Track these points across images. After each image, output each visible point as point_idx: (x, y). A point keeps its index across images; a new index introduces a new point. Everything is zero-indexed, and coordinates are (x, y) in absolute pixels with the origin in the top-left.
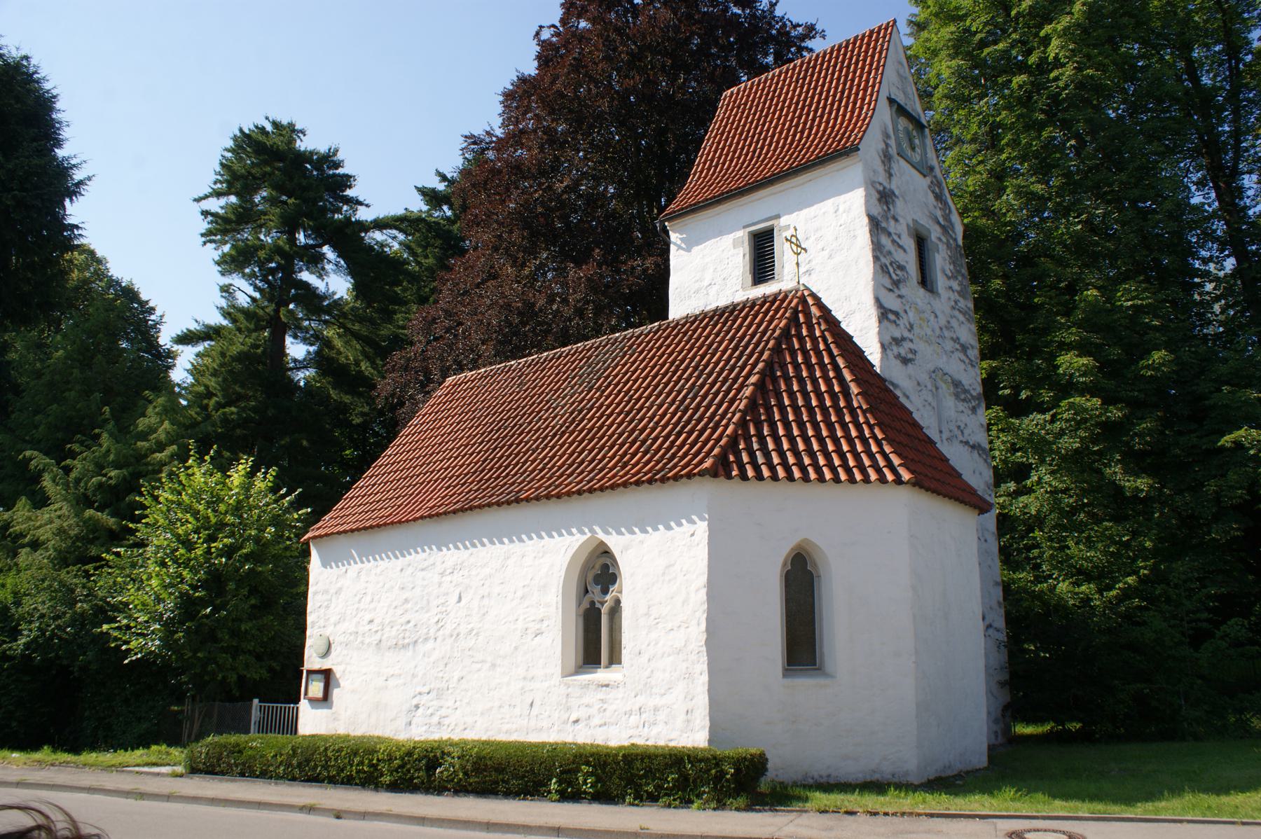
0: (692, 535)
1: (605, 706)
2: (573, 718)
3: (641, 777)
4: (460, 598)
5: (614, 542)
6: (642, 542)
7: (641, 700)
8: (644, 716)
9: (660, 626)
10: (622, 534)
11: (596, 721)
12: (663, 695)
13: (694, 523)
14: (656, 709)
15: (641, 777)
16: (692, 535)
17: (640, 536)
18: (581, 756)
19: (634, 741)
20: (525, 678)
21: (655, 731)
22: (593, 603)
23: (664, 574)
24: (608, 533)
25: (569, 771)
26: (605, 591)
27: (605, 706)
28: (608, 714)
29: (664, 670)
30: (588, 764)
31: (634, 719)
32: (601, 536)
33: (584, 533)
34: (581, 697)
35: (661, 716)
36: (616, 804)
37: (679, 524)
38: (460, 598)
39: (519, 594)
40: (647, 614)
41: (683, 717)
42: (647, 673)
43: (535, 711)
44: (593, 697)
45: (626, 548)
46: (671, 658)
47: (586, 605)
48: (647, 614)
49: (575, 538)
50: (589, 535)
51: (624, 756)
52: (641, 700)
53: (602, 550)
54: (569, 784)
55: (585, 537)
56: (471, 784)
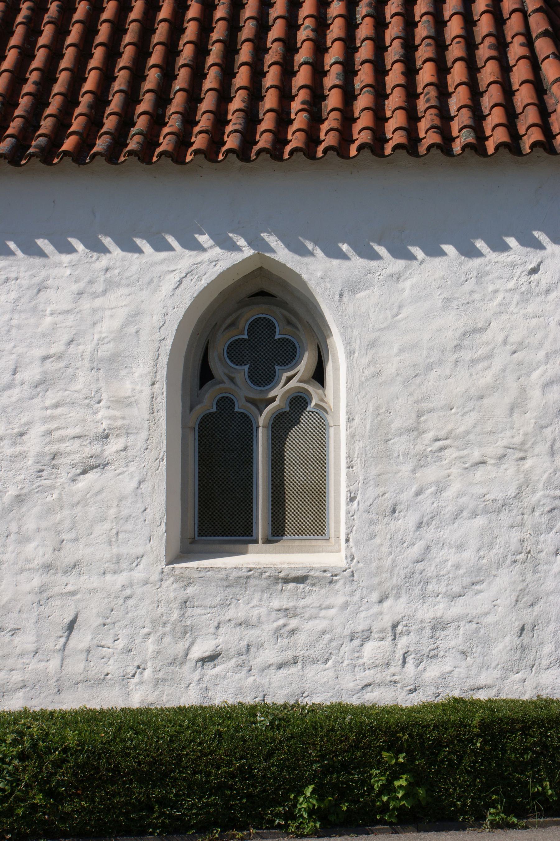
0: (534, 271)
1: (293, 623)
2: (201, 649)
3: (522, 767)
4: (415, 376)
5: (319, 273)
6: (397, 277)
7: (395, 608)
8: (403, 642)
9: (450, 454)
10: (344, 257)
11: (269, 655)
12: (454, 597)
13: (540, 246)
14: (438, 626)
15: (522, 767)
16: (534, 271)
17: (391, 264)
18: (373, 731)
19: (240, 699)
20: (48, 567)
21: (433, 672)
22: (226, 403)
23: (458, 347)
24: (302, 251)
25: (345, 767)
26: (264, 377)
27: (293, 623)
28: (301, 638)
29: (461, 547)
30: (394, 746)
31: (371, 649)
32: (282, 254)
33: (235, 248)
34: (224, 605)
35: (451, 640)
36: (462, 827)
37: (500, 247)
38: (415, 376)
39: (31, 373)
40: (416, 430)
41: (510, 639)
42: (416, 550)
43: (81, 639)
44: (256, 605)
45: (353, 287)
46: (480, 521)
47: (208, 403)
48: (416, 430)
49: (205, 256)
50: (248, 252)
51: (483, 725)
52: (395, 608)
53: (252, 288)
54: (344, 792)
55: (237, 257)
56: (65, 817)
